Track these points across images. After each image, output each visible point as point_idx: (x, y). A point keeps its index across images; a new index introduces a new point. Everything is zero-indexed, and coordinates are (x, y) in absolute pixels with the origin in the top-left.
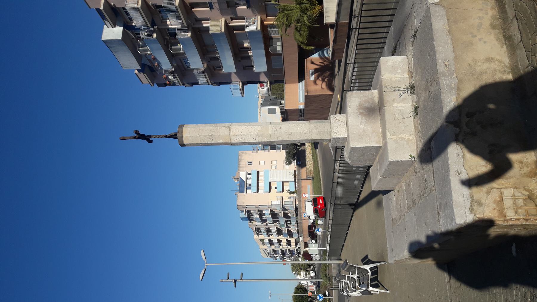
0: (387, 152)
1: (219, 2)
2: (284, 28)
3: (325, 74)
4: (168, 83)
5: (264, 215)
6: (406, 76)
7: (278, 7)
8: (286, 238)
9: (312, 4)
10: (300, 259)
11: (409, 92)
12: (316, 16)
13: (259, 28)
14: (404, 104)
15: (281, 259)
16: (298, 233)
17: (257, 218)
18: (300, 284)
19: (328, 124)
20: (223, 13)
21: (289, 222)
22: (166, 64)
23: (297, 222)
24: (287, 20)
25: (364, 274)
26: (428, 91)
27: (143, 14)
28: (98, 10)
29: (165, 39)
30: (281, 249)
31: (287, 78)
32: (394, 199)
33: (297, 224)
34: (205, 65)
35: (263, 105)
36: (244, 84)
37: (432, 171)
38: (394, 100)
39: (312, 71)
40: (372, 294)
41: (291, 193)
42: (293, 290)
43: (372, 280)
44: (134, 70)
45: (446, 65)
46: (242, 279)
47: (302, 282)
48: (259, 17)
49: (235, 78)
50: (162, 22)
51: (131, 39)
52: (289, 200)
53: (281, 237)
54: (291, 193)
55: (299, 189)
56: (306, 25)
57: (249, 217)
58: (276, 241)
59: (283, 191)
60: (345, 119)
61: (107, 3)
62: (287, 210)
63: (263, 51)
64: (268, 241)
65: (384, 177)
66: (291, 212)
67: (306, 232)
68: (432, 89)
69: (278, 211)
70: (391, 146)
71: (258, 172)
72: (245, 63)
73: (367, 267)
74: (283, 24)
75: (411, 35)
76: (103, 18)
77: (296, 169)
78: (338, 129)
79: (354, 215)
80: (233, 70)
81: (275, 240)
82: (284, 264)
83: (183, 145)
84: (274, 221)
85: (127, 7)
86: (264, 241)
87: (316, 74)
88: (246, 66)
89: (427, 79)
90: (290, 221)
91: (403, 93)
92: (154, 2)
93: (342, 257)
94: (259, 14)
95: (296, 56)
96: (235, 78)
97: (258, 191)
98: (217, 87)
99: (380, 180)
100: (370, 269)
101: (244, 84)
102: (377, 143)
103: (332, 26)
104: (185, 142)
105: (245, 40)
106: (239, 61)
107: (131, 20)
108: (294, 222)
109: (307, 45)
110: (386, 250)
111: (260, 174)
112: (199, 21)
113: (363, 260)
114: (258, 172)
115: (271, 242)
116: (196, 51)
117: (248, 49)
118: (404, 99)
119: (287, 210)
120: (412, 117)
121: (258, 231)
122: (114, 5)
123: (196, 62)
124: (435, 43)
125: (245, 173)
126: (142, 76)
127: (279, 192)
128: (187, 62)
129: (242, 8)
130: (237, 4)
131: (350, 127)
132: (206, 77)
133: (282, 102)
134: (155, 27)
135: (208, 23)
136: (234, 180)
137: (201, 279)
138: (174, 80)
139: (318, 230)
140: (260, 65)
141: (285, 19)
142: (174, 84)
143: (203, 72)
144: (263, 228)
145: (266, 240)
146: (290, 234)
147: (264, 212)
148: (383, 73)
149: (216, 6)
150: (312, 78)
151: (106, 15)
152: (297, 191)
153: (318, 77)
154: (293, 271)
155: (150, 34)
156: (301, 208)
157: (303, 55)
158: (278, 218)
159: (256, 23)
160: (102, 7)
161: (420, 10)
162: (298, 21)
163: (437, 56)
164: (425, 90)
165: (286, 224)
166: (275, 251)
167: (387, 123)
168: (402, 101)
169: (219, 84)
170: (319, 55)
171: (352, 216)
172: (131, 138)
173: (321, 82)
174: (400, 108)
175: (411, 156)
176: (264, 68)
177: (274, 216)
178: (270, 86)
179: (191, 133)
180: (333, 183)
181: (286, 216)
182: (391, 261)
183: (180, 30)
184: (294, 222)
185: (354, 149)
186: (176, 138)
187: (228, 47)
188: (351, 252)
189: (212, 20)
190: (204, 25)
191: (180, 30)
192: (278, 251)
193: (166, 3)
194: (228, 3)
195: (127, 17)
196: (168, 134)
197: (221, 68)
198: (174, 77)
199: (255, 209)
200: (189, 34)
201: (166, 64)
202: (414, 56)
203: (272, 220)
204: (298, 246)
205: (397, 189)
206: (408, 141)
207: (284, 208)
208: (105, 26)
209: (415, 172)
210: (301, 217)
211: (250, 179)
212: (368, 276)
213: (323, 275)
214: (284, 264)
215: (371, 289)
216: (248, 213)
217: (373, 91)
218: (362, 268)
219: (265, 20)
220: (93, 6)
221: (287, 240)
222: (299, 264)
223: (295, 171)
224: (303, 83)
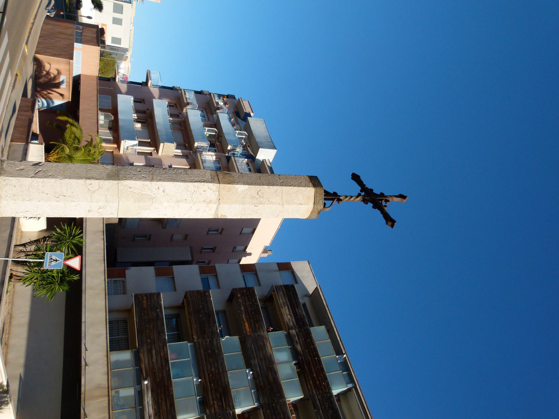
2: (94, 143)
3: (46, 79)
12: (55, 151)
22: (224, 118)
24: (90, 151)
29: (220, 142)
31: (95, 83)
36: (146, 84)
39: (63, 86)
44: (254, 116)
48: (121, 152)
49: (155, 92)
50: (220, 159)
56: (66, 144)
63: (120, 117)
72: (141, 107)
76: (271, 169)
87: (57, 81)
88: (141, 102)
94: (121, 156)
96: (155, 92)
98: (176, 85)
101: (146, 84)
103: (35, 137)
107: (247, 164)
109: (67, 122)
112: (185, 156)
116: (192, 127)
117: (137, 121)
123: (194, 116)
126: (247, 109)
128: (203, 116)
132: (186, 98)
134: (227, 155)
140: (126, 103)
141: (92, 151)
142: (220, 96)
150: (62, 78)
151: (268, 170)
153: (55, 78)
157: (72, 108)
159: (126, 147)
162: (77, 149)
169: (172, 89)
170: (53, 103)
173: (51, 71)
183: (204, 149)
189: (172, 154)
190: (180, 151)
197: (169, 106)
198: (217, 103)
200: (196, 144)
201: (224, 118)
208: (271, 161)
219: (116, 148)
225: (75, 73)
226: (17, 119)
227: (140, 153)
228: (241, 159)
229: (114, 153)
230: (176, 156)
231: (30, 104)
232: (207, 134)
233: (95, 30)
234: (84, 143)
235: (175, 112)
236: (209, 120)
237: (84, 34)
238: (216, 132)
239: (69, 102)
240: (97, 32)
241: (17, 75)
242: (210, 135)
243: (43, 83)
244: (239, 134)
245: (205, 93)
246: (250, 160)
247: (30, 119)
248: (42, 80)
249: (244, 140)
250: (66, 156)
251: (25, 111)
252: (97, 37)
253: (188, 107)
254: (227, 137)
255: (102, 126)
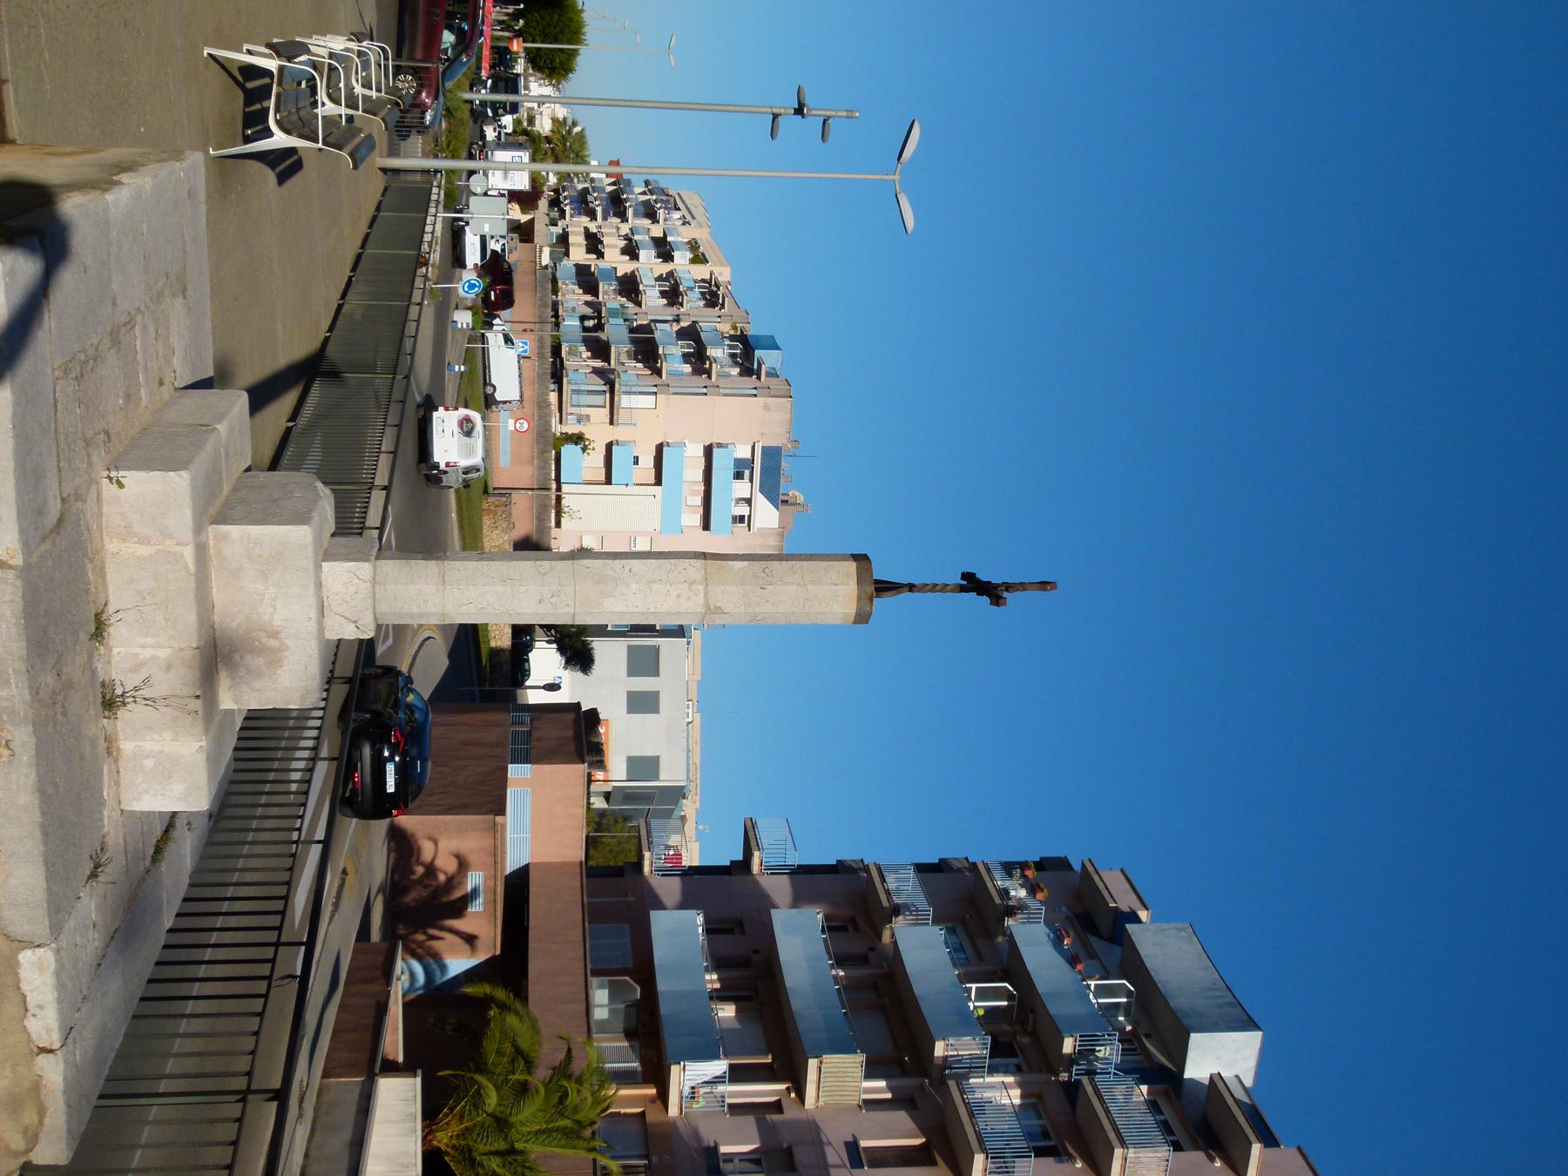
0: (194, 500)
1: (824, 1167)
2: (578, 1066)
3: (425, 893)
4: (1029, 873)
5: (686, 358)
6: (126, 746)
7: (598, 1143)
8: (602, 264)
9: (468, 1157)
10: (553, 180)
11: (119, 692)
12: (452, 1109)
13: (675, 1069)
14: (137, 655)
15: (628, 183)
16: (554, 281)
17: (717, 344)
18: (557, 87)
19: (383, 608)
20: (812, 1132)
21: (590, 323)
22: (1033, 940)
23: (557, 325)
24: (565, 1095)
25: (294, 118)
26: (64, 677)
27: (1102, 1115)
28: (1270, 1141)
29: (1033, 1034)
30: (624, 219)
31: (573, 886)
32: (176, 362)
33: (556, 316)
34: (886, 938)
35: (678, 794)
36: (743, 866)
37: (61, 429)
38: (169, 667)
39: (477, 907)
40: (270, 46)
41: (578, 439)
42: (581, 61)
43: (265, 92)
44: (1153, 919)
45: (7, 746)
46: (775, 116)
47: (548, 91)
48: (673, 1111)
49: (779, 888)
50: (1040, 1096)
51: (1156, 1035)
52: (585, 411)
53: (625, 266)
54: (578, 439)
55: (543, 452)
56: (490, 1074)
57: (746, 352)
58: (643, 254)
59: (609, 447)
60: (328, 622)
61: (1237, 1164)
62: (596, 371)
63: (663, 985)
64: (676, 254)
65: (206, 428)
66: (580, 363)
67: (521, 281)
68: (50, 679)
69: (631, 371)
70: (182, 518)
71: (706, 526)
72: (733, 945)
73: (279, 139)
74: (579, 1081)
75: (108, 869)
76: (1253, 1113)
77: (554, 532)
78: (352, 589)
79: (323, 334)
80: (782, 918)
81: (647, 255)
82: (617, 163)
83: (861, 559)
84: (647, 329)
85: (1164, 1152)
86: (689, 255)
87: (457, 894)
88: (730, 931)
89: (65, 714)
90: (585, 329)
91: (136, 689)
92: (1066, 1166)
93: (379, 182)
94: (673, 1125)
95: (537, 965)
96: (779, 888)
97: (708, 452)
98: (848, 855)
99: (220, 418)
100: (271, 135)
101: (743, 866)
102: (226, 537)
103: (391, 1068)
104: (852, 566)
105: (731, 1031)
106: (756, 952)
107: (1153, 1105)
108: (571, 323)
109: (487, 1001)
110: (209, 196)
111: (696, 519)
112: (900, 1101)
113: (298, 166)
114: (706, 526)
115: (664, 250)
116: (919, 988)
117: (720, 996)
118: (134, 669)
119: (596, 371)
120: (111, 609)
121: (714, 295)
122: (1212, 1159)
123: (922, 947)
124: (38, 818)
125: (757, 523)
126: (1123, 899)
127: (625, 443)
128: (956, 950)
129: (738, 1144)
130: (757, 1162)
131: (311, 590)
132: (888, 892)
133: (599, 803)
134: (1064, 1076)
135: (867, 1091)
136: (801, 499)
137: (916, 126)
138: (1007, 884)
139: (472, 286)
140: (678, 934)
141: (573, 1098)
142: (1008, 868)
143: (896, 910)
144: (692, 303)
145: (681, 258)
146: (587, 279)
147: (687, 368)
148: (202, 757)
149: (835, 1155)
150: (474, 879)
151: (1242, 1120)
152: (551, 446)
153: (452, 883)
154: (581, 135)
155: (1085, 1053)
156: (541, 376)
157: (509, 967)
158: (633, 341)
159: (687, 1091)
160: (1256, 1148)
161: (78, 940)
162: (523, 1090)
163: (33, 776)
164: (69, 686)
165: (599, 317)
166: (651, 215)
167: (192, 594)
168: (143, 664)
169: (839, 868)
170: (443, 968)
171: (331, 329)
172: (1022, 586)
173: (439, 863)
174: (151, 641)
175: (121, 485)
176: (661, 922)
177: (646, 350)
178: (641, 857)
179: (832, 594)
180: (394, 453)
181: (600, 349)
182: (195, 159)
183: (973, 1067)
184: (571, 323)
185: (301, 519)
186: (877, 582)
187: (796, 1004)
188: (343, 198)
189: (854, 1100)
190: (882, 1084)
191: (973, 1067)
192: (636, 215)
193: (1019, 1162)
194: (791, 1165)
195: (1168, 1114)
196: (906, 596)
197: (831, 927)
198: (1004, 893)
199: (721, 382)
200: (940, 1049)
201: (1033, 940)
202: (101, 803)
203: (657, 335)
204: (557, 230)
205: (166, 392)
206: (126, 534)
207: (608, 378)
208: (1248, 1083)
209: (107, 433)
210: (541, 340)
211: (739, 500)
212: (277, 110)
213: (459, 115)
214: (617, 163)
215: (272, 64)
216: (748, 368)
217: (235, 707)
218: (301, 136)
219: (652, 1100)
220: (1286, 1155)
221: (600, 255)
222: (557, 161)
223: (558, 525)
224: (511, 865)
225: (513, 861)
226: (342, 1007)
227: (736, 1109)
228: (1119, 1091)
229: (650, 1118)
230: (869, 1104)
231: (381, 960)
232: (977, 1006)
233: (570, 717)
234: (541, 1074)
235: (856, 946)
236: (980, 959)
237: (536, 734)
238: (1010, 997)
239: (494, 957)
240: (577, 721)
241: (344, 872)
242: (990, 1011)
243: (418, 904)
244: (1102, 991)
245: (956, 865)
246: (1162, 1087)
247: (378, 1003)
248: (411, 897)
249: (1127, 1015)
250: (489, 1121)
251: (365, 982)
252: (577, 738)
253: (899, 923)
254: (1053, 1008)
255: (604, 1026)
